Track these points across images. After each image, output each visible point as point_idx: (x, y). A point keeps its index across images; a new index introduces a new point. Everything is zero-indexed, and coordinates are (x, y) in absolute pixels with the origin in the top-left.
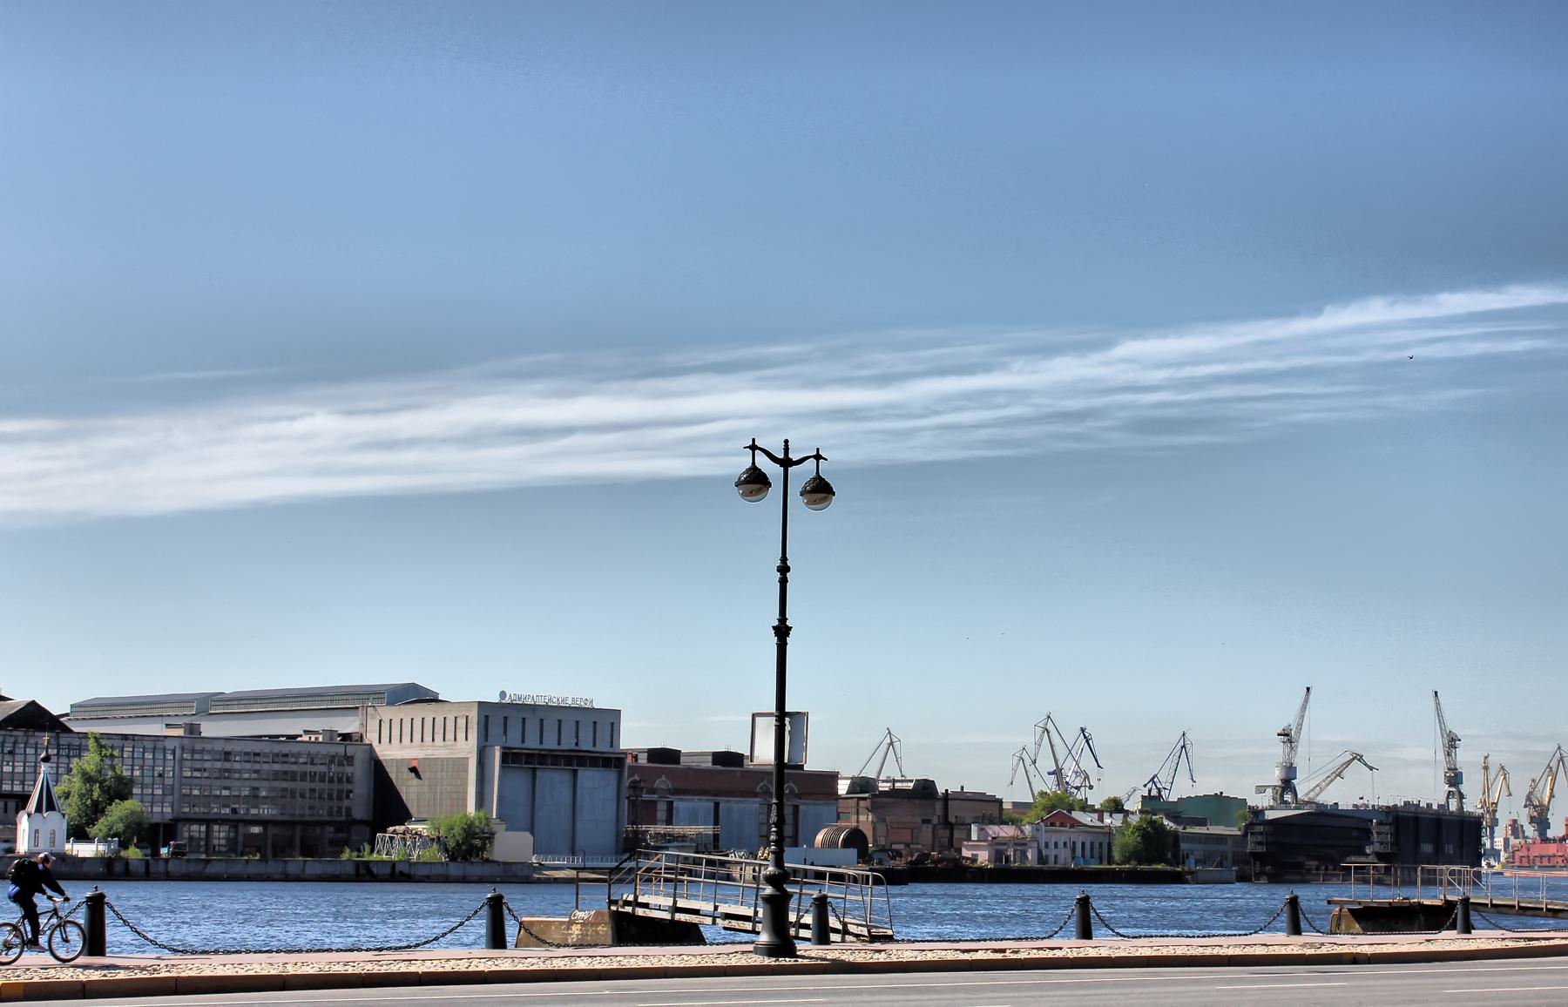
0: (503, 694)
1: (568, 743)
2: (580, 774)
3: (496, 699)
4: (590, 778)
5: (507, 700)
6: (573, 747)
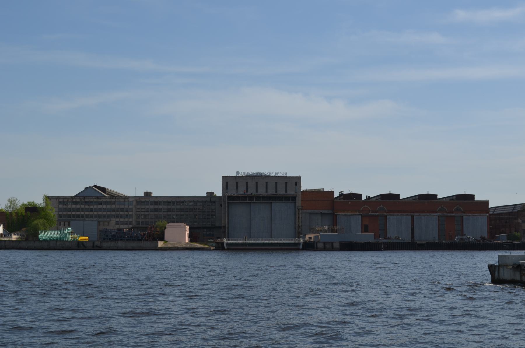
0: (238, 173)
1: (271, 191)
2: (273, 205)
3: (235, 175)
4: (277, 206)
5: (240, 175)
6: (275, 193)
